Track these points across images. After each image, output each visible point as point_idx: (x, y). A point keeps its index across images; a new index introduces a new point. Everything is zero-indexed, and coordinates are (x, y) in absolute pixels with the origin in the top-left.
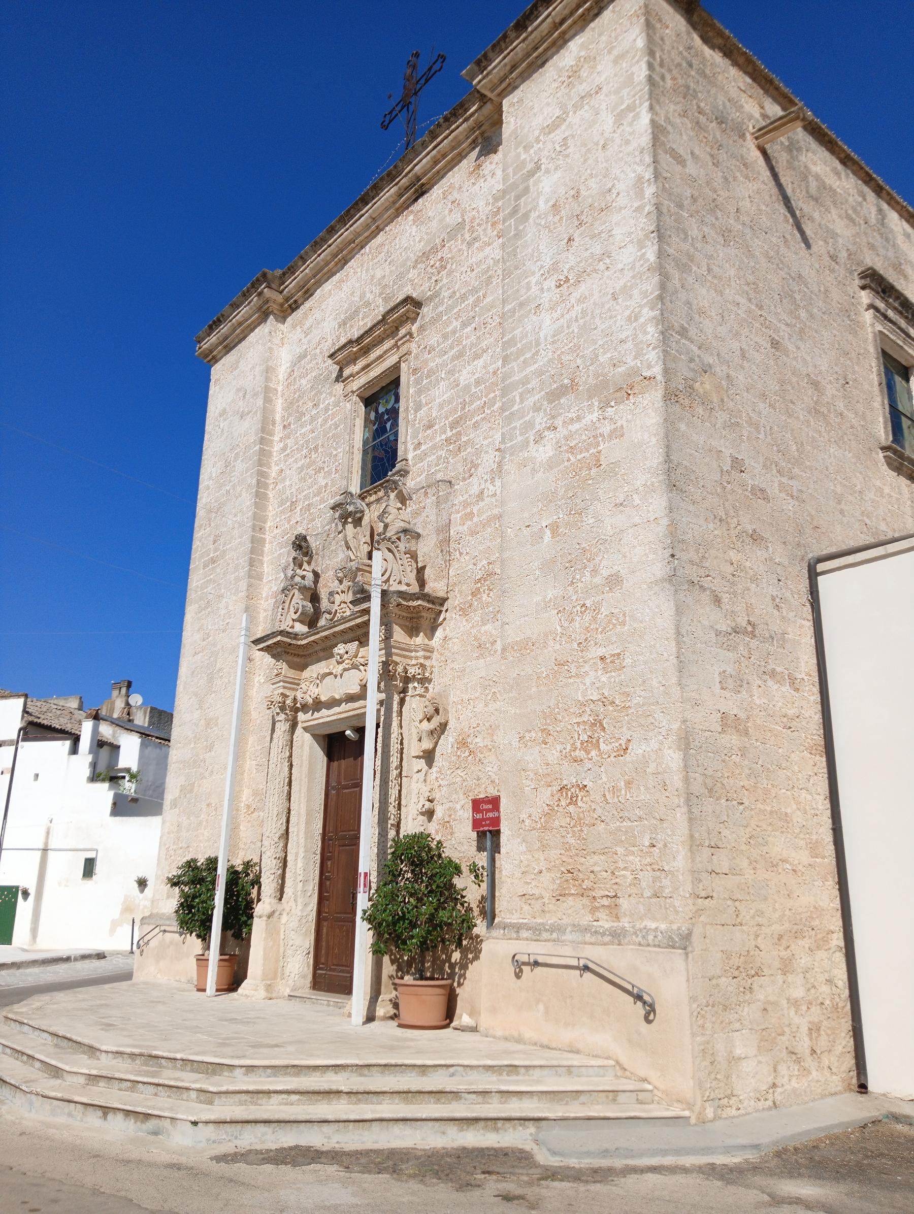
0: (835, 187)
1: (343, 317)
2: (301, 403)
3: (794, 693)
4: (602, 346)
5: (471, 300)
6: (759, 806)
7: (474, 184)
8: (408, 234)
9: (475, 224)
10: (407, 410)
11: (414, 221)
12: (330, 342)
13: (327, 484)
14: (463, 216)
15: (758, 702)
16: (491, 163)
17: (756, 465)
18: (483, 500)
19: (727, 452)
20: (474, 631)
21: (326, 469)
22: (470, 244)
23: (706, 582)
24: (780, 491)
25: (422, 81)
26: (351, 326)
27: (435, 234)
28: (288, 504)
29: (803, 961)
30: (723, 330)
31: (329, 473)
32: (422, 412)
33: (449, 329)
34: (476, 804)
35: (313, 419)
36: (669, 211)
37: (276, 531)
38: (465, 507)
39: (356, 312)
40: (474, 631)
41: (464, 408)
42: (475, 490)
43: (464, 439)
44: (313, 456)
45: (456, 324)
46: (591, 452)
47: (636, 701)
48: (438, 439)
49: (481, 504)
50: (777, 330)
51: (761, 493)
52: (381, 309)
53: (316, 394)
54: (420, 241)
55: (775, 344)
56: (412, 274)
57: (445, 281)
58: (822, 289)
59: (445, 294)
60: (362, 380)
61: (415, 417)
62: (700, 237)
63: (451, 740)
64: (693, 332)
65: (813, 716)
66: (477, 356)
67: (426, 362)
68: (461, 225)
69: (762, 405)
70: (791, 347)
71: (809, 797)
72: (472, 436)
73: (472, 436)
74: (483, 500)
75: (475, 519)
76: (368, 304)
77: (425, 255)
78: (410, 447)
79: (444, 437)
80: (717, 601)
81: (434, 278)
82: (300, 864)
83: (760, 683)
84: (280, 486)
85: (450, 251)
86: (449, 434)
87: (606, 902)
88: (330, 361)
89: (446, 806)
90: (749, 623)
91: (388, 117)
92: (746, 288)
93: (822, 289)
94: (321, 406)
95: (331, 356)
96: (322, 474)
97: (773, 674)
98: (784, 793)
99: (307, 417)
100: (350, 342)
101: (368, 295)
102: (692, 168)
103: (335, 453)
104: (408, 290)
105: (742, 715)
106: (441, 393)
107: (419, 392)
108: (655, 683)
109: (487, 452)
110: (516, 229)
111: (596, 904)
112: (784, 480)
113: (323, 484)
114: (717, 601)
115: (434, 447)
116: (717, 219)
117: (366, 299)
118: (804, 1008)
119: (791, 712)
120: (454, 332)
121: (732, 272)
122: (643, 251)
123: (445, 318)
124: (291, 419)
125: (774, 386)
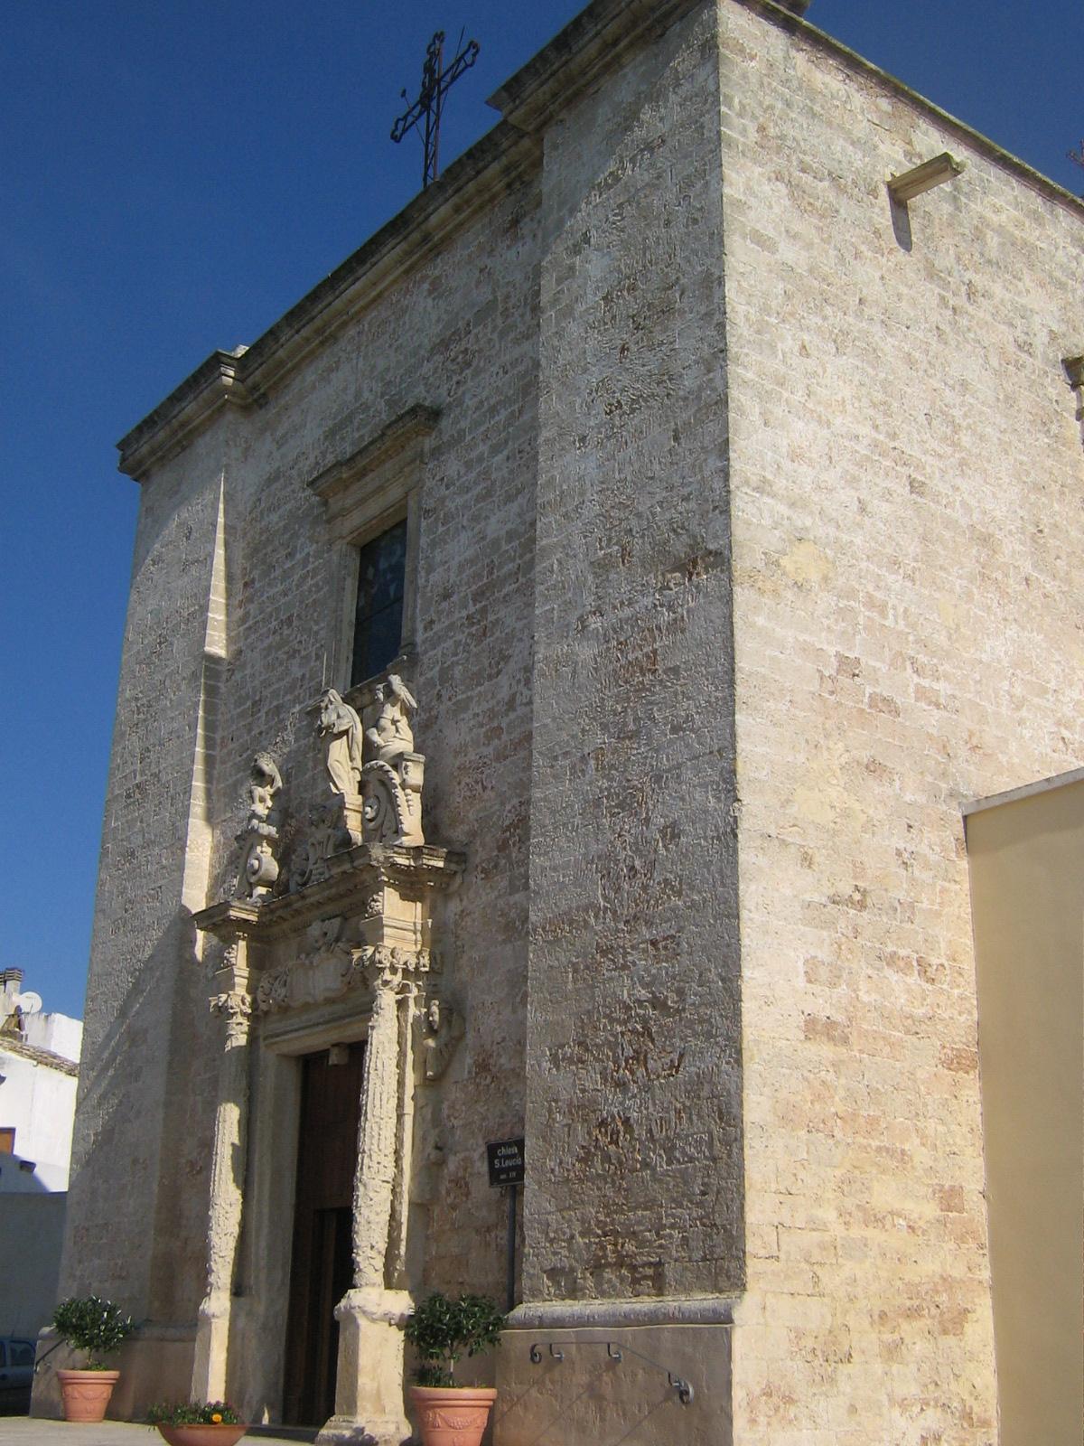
0: (1032, 239)
1: (330, 423)
2: (270, 549)
3: (930, 987)
4: (661, 503)
5: (503, 415)
6: (860, 1140)
7: (509, 247)
8: (421, 310)
9: (510, 305)
10: (415, 570)
11: (430, 292)
12: (312, 460)
13: (304, 675)
14: (494, 291)
15: (865, 998)
16: (532, 220)
17: (878, 665)
18: (515, 710)
19: (832, 650)
20: (501, 903)
21: (303, 653)
22: (502, 335)
23: (792, 837)
24: (917, 700)
25: (448, 78)
26: (343, 439)
27: (457, 314)
28: (249, 703)
29: (917, 1347)
30: (831, 477)
31: (307, 658)
32: (435, 574)
33: (473, 455)
34: (492, 1150)
35: (286, 575)
36: (748, 320)
37: (231, 746)
38: (491, 719)
39: (350, 418)
40: (501, 903)
41: (492, 573)
42: (504, 694)
43: (492, 618)
44: (286, 632)
45: (483, 448)
46: (849, 539)
47: (690, 1001)
48: (457, 615)
49: (512, 716)
50: (920, 467)
51: (885, 705)
52: (384, 416)
53: (291, 538)
54: (438, 321)
55: (915, 487)
56: (427, 368)
57: (470, 384)
58: (1001, 397)
59: (470, 403)
60: (355, 520)
61: (427, 581)
62: (796, 349)
63: (469, 1061)
64: (780, 484)
65: (956, 1016)
66: (510, 499)
67: (442, 500)
68: (491, 305)
69: (891, 578)
70: (943, 488)
71: (941, 1129)
72: (501, 614)
73: (501, 614)
74: (515, 710)
75: (505, 737)
76: (365, 407)
77: (444, 344)
78: (420, 626)
79: (464, 613)
80: (807, 860)
81: (455, 379)
82: (263, 1244)
83: (870, 972)
84: (238, 676)
85: (477, 340)
86: (472, 609)
87: (649, 1271)
88: (309, 492)
89: (460, 1156)
90: (857, 888)
91: (401, 123)
92: (871, 412)
93: (1001, 397)
94: (298, 556)
95: (311, 484)
96: (296, 661)
97: (892, 960)
98: (902, 1123)
99: (278, 572)
100: (338, 464)
101: (366, 394)
102: (789, 253)
103: (315, 628)
104: (419, 394)
105: (839, 1017)
106: (460, 548)
107: (433, 545)
108: (712, 976)
109: (521, 640)
110: (558, 323)
111: (637, 1276)
112: (926, 683)
113: (299, 675)
114: (807, 860)
115: (451, 627)
116: (825, 318)
117: (363, 400)
118: (916, 1409)
119: (920, 1012)
120: (480, 459)
121: (846, 392)
122: (711, 375)
123: (468, 438)
124: (256, 574)
125: (913, 548)
